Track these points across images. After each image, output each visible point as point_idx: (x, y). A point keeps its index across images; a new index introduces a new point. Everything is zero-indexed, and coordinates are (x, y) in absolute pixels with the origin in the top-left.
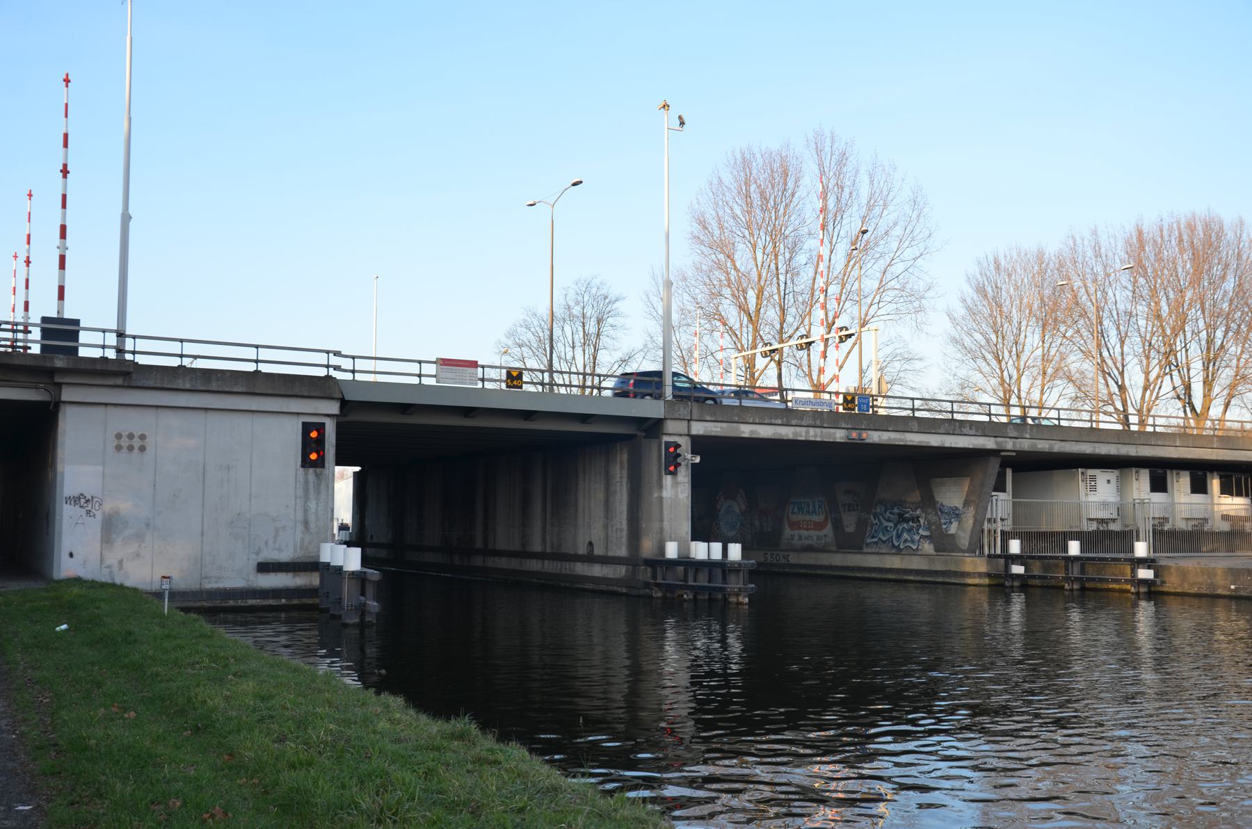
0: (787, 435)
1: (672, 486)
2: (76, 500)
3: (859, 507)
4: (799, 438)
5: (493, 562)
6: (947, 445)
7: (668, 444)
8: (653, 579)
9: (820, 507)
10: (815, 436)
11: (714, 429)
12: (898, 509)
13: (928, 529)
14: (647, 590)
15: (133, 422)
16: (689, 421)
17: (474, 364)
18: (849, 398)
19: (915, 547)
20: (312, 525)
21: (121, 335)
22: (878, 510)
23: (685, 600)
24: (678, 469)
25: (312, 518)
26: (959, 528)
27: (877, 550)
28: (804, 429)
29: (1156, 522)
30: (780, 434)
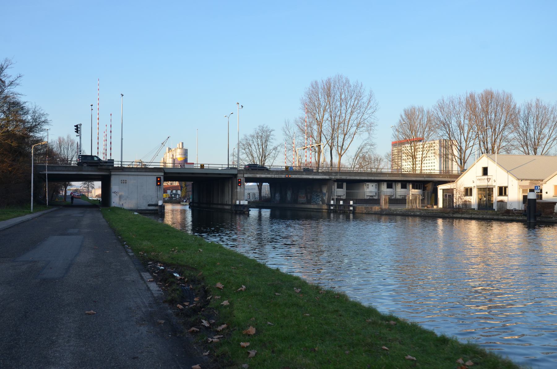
2: (114, 192)
5: (215, 206)
6: (314, 178)
7: (239, 179)
15: (124, 178)
17: (193, 164)
20: (159, 197)
21: (122, 162)
25: (159, 196)
29: (389, 196)
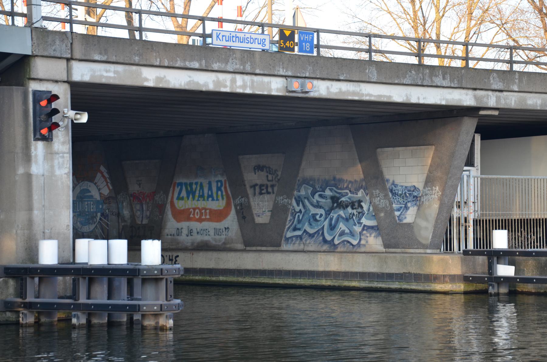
0: (206, 84)
1: (45, 158)
3: (276, 189)
4: (223, 90)
6: (414, 100)
8: (21, 297)
9: (219, 189)
10: (244, 86)
11: (105, 74)
12: (331, 190)
13: (375, 217)
14: (9, 314)
16: (68, 60)
18: (287, 33)
19: (355, 242)
22: (303, 193)
23: (74, 327)
24: (54, 132)
26: (418, 215)
27: (301, 247)
28: (228, 77)
30: (198, 83)
